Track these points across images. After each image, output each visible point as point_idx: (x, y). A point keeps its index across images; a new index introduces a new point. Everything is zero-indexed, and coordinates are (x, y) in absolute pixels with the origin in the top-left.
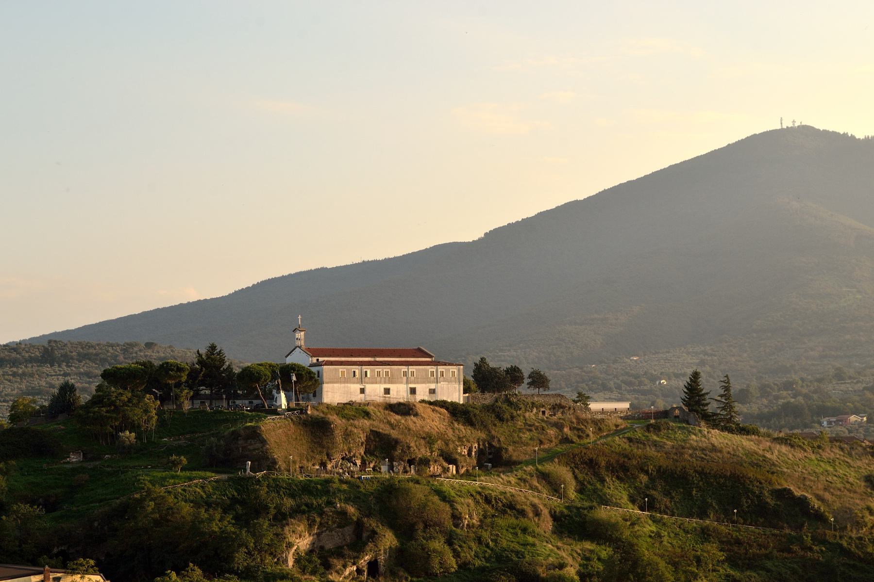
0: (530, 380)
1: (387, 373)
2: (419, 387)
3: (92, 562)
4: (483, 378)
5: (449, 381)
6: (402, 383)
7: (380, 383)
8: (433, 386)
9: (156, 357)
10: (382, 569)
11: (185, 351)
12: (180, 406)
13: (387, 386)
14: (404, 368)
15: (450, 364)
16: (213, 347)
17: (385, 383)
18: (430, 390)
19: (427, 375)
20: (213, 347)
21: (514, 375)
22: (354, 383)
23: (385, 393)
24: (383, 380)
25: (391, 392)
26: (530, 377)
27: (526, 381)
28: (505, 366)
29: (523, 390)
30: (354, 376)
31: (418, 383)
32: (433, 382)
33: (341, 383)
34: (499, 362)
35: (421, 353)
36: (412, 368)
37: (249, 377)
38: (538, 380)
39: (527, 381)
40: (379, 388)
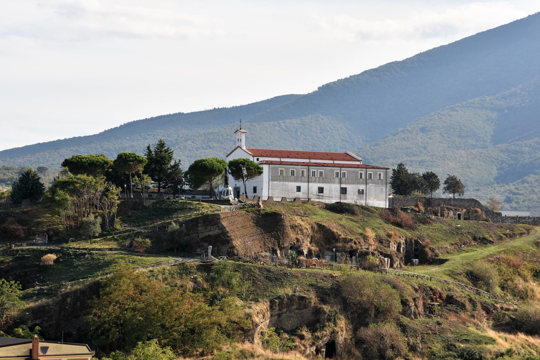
0: (446, 186)
1: (321, 173)
2: (350, 188)
3: (282, 331)
4: (402, 183)
5: (376, 183)
6: (334, 183)
7: (315, 182)
8: (362, 187)
9: (244, 160)
10: (339, 349)
11: (139, 147)
12: (216, 198)
13: (321, 185)
14: (337, 170)
15: (377, 168)
16: (161, 145)
17: (319, 182)
18: (359, 190)
19: (357, 177)
20: (161, 145)
21: (430, 181)
22: (291, 181)
23: (319, 192)
24: (317, 179)
25: (324, 191)
26: (446, 182)
27: (442, 186)
28: (422, 171)
29: (440, 193)
30: (303, 175)
31: (348, 183)
32: (362, 183)
33: (280, 180)
34: (416, 169)
35: (346, 157)
36: (344, 170)
37: (202, 171)
38: (453, 185)
39: (442, 186)
40: (314, 187)
